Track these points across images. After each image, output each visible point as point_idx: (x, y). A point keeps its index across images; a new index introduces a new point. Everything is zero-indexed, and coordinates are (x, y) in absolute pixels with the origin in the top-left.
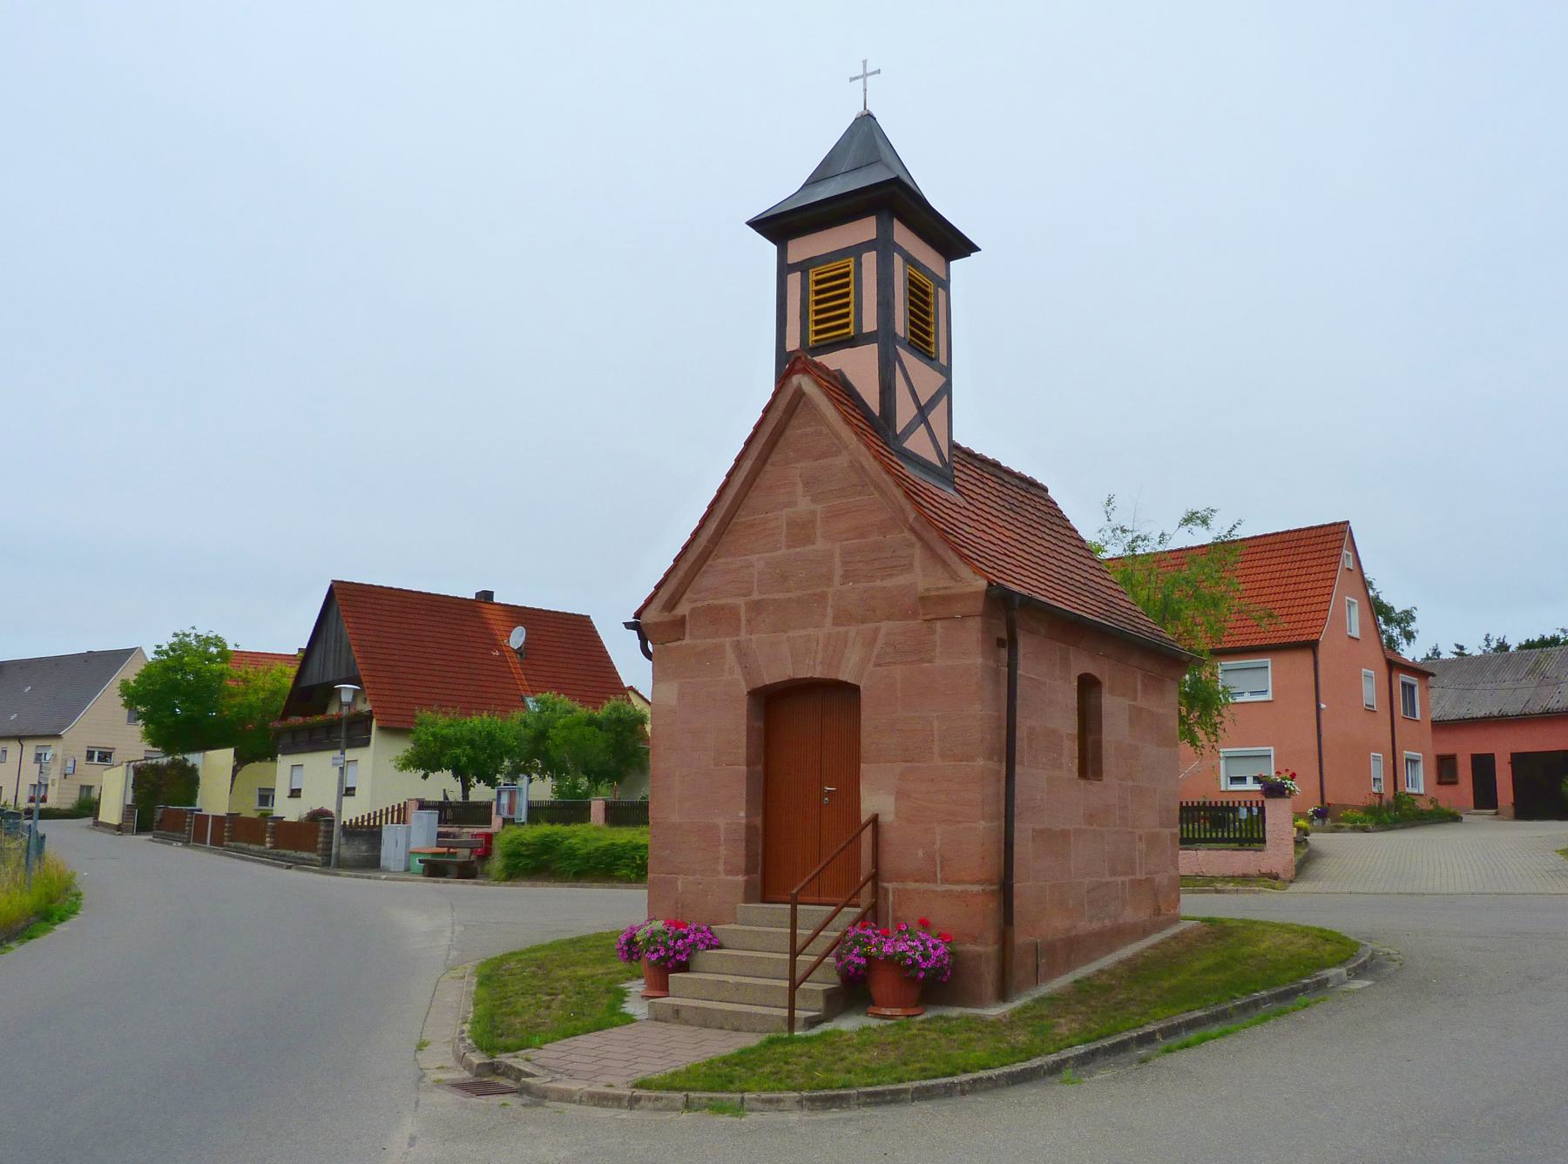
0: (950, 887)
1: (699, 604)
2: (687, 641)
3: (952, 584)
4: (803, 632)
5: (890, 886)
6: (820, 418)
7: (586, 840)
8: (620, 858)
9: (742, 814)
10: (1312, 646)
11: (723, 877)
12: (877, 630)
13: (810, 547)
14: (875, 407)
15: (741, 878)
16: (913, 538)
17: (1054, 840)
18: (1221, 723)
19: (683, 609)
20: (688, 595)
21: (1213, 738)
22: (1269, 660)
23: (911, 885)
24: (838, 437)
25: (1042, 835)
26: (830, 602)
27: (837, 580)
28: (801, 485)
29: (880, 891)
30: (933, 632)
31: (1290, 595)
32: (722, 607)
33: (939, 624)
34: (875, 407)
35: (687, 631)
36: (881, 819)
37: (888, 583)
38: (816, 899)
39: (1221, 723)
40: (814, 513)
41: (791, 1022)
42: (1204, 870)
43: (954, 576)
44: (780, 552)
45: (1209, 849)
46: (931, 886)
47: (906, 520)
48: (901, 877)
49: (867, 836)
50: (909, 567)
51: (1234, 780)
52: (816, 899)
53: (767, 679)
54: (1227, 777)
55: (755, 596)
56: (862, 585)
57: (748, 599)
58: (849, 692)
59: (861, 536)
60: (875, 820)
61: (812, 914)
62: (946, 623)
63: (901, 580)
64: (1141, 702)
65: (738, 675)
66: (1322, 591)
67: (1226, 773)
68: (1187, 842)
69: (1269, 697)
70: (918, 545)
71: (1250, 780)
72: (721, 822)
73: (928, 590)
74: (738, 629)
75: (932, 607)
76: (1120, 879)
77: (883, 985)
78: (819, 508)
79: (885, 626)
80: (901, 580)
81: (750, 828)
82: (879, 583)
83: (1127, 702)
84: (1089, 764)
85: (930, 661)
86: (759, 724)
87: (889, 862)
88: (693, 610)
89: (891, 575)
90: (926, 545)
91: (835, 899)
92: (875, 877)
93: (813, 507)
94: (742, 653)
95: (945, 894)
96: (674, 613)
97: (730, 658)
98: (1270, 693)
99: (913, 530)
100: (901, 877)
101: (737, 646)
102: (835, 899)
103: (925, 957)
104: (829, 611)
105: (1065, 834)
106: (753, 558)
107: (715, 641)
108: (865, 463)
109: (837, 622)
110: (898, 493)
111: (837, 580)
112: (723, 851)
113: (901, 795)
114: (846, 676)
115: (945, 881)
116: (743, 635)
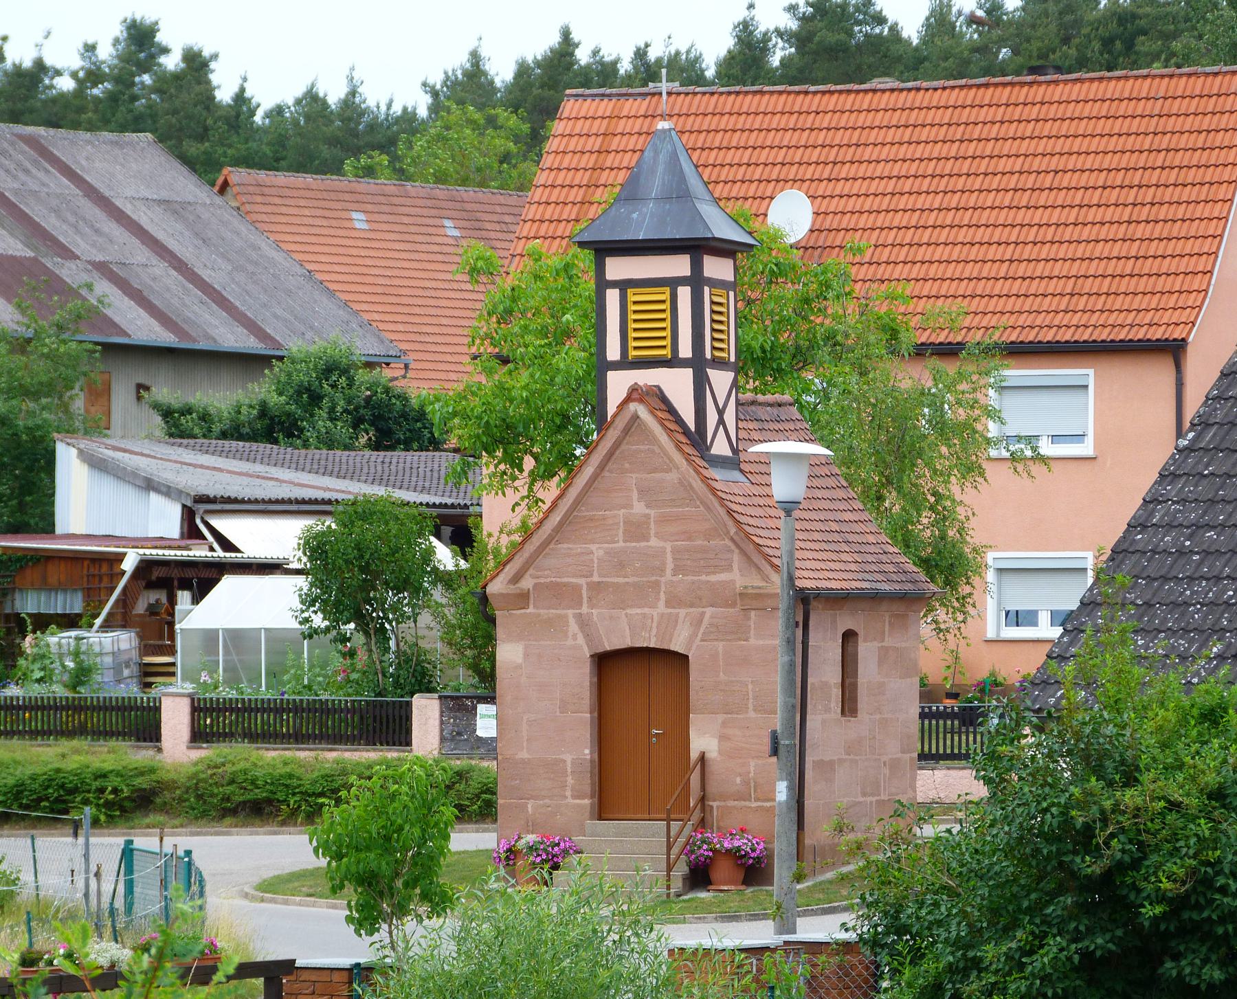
0: (760, 804)
1: (542, 580)
2: (531, 610)
3: (763, 584)
4: (639, 611)
5: (715, 804)
6: (651, 439)
7: (255, 765)
8: (74, 791)
9: (587, 751)
10: (1174, 350)
11: (570, 800)
12: (703, 614)
13: (643, 544)
14: (692, 426)
15: (587, 802)
16: (733, 547)
17: (827, 767)
18: (970, 594)
19: (527, 583)
20: (531, 571)
21: (960, 617)
22: (1091, 372)
23: (731, 803)
24: (671, 460)
25: (819, 764)
26: (663, 589)
27: (669, 572)
28: (635, 491)
29: (707, 809)
30: (749, 619)
31: (1140, 230)
32: (565, 585)
33: (753, 613)
34: (692, 426)
35: (531, 601)
36: (707, 755)
37: (713, 578)
38: (647, 816)
39: (970, 594)
40: (647, 516)
41: (668, 895)
42: (942, 795)
43: (766, 578)
44: (616, 545)
45: (948, 769)
46: (747, 803)
47: (728, 532)
48: (723, 797)
49: (695, 778)
50: (729, 568)
51: (1017, 618)
52: (647, 816)
53: (608, 646)
54: (999, 610)
55: (596, 578)
56: (690, 578)
57: (589, 580)
58: (681, 660)
59: (690, 539)
60: (702, 758)
61: (675, 826)
62: (758, 612)
63: (723, 577)
64: (888, 642)
65: (581, 640)
66: (1195, 246)
67: (999, 604)
68: (928, 758)
69: (1086, 448)
70: (737, 551)
71: (1044, 618)
72: (568, 758)
73: (746, 587)
74: (580, 605)
75: (750, 600)
76: (869, 799)
77: (722, 870)
78: (652, 512)
79: (709, 611)
80: (723, 577)
81: (592, 761)
82: (704, 578)
83: (876, 644)
84: (849, 705)
85: (746, 640)
86: (595, 679)
87: (712, 788)
88: (536, 585)
89: (714, 573)
90: (743, 553)
91: (681, 816)
92: (703, 799)
93: (647, 511)
94: (584, 623)
95: (757, 809)
96: (517, 585)
97: (573, 627)
98: (1090, 440)
99: (732, 539)
100: (723, 797)
101: (579, 617)
102: (681, 816)
103: (753, 850)
104: (662, 596)
105: (832, 763)
106: (593, 547)
107: (558, 612)
108: (694, 485)
109: (668, 604)
110: (722, 512)
111: (669, 572)
112: (570, 781)
113: (723, 738)
114: (677, 646)
115: (757, 800)
116: (585, 609)
